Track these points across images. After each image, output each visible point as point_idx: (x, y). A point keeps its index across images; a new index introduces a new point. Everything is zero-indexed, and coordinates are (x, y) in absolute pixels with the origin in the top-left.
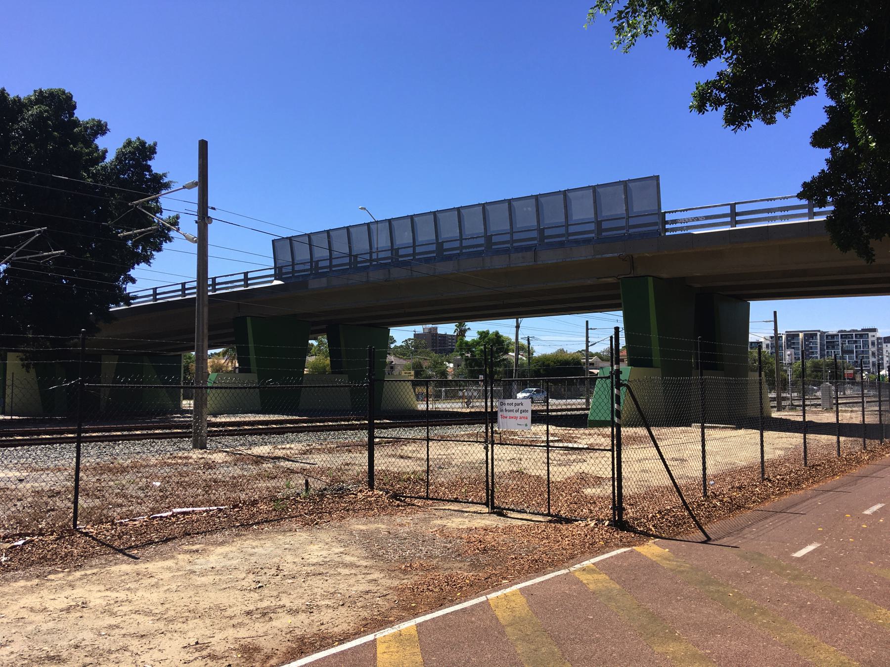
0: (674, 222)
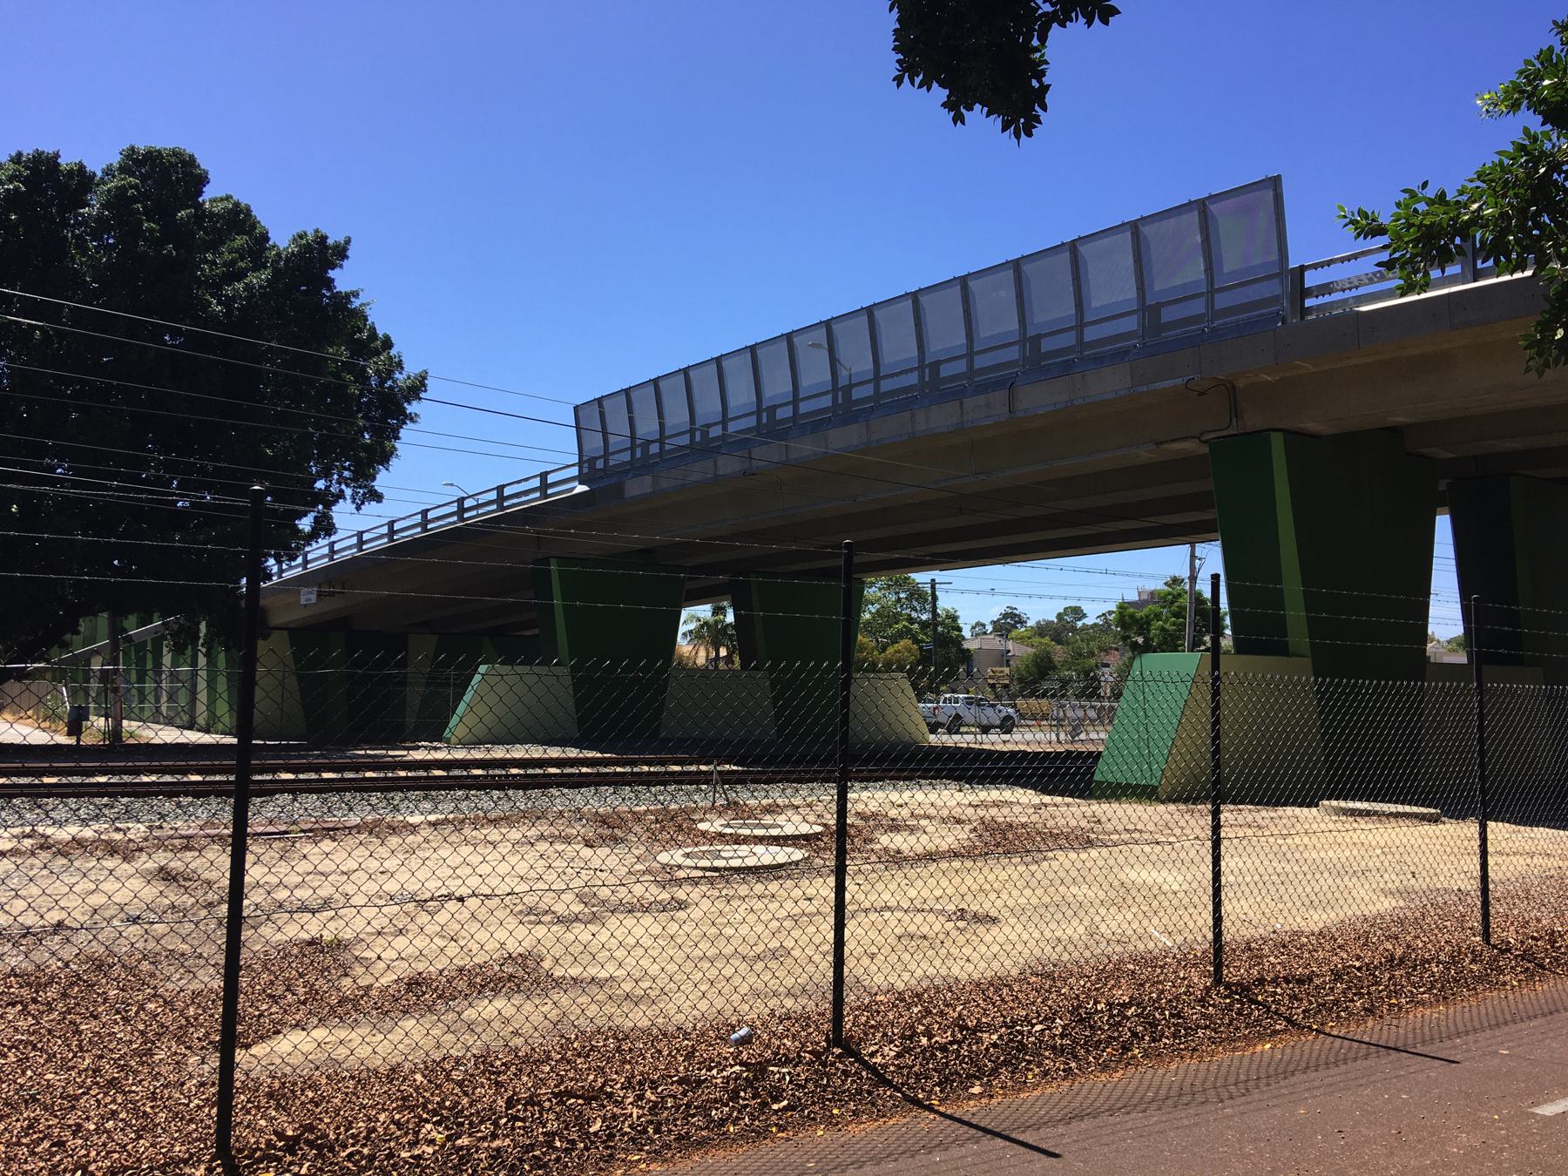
0: (1326, 289)
